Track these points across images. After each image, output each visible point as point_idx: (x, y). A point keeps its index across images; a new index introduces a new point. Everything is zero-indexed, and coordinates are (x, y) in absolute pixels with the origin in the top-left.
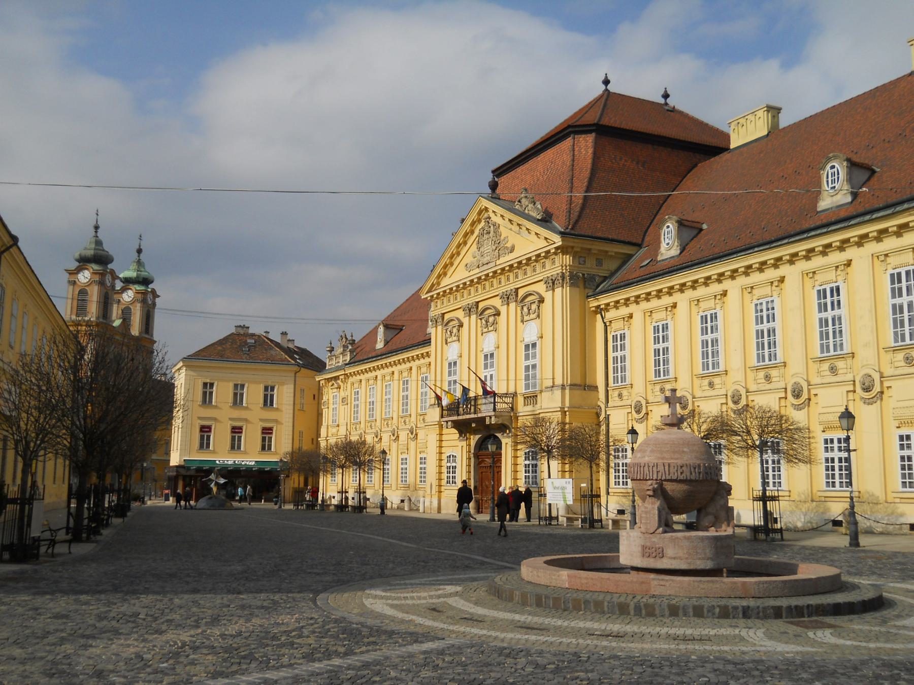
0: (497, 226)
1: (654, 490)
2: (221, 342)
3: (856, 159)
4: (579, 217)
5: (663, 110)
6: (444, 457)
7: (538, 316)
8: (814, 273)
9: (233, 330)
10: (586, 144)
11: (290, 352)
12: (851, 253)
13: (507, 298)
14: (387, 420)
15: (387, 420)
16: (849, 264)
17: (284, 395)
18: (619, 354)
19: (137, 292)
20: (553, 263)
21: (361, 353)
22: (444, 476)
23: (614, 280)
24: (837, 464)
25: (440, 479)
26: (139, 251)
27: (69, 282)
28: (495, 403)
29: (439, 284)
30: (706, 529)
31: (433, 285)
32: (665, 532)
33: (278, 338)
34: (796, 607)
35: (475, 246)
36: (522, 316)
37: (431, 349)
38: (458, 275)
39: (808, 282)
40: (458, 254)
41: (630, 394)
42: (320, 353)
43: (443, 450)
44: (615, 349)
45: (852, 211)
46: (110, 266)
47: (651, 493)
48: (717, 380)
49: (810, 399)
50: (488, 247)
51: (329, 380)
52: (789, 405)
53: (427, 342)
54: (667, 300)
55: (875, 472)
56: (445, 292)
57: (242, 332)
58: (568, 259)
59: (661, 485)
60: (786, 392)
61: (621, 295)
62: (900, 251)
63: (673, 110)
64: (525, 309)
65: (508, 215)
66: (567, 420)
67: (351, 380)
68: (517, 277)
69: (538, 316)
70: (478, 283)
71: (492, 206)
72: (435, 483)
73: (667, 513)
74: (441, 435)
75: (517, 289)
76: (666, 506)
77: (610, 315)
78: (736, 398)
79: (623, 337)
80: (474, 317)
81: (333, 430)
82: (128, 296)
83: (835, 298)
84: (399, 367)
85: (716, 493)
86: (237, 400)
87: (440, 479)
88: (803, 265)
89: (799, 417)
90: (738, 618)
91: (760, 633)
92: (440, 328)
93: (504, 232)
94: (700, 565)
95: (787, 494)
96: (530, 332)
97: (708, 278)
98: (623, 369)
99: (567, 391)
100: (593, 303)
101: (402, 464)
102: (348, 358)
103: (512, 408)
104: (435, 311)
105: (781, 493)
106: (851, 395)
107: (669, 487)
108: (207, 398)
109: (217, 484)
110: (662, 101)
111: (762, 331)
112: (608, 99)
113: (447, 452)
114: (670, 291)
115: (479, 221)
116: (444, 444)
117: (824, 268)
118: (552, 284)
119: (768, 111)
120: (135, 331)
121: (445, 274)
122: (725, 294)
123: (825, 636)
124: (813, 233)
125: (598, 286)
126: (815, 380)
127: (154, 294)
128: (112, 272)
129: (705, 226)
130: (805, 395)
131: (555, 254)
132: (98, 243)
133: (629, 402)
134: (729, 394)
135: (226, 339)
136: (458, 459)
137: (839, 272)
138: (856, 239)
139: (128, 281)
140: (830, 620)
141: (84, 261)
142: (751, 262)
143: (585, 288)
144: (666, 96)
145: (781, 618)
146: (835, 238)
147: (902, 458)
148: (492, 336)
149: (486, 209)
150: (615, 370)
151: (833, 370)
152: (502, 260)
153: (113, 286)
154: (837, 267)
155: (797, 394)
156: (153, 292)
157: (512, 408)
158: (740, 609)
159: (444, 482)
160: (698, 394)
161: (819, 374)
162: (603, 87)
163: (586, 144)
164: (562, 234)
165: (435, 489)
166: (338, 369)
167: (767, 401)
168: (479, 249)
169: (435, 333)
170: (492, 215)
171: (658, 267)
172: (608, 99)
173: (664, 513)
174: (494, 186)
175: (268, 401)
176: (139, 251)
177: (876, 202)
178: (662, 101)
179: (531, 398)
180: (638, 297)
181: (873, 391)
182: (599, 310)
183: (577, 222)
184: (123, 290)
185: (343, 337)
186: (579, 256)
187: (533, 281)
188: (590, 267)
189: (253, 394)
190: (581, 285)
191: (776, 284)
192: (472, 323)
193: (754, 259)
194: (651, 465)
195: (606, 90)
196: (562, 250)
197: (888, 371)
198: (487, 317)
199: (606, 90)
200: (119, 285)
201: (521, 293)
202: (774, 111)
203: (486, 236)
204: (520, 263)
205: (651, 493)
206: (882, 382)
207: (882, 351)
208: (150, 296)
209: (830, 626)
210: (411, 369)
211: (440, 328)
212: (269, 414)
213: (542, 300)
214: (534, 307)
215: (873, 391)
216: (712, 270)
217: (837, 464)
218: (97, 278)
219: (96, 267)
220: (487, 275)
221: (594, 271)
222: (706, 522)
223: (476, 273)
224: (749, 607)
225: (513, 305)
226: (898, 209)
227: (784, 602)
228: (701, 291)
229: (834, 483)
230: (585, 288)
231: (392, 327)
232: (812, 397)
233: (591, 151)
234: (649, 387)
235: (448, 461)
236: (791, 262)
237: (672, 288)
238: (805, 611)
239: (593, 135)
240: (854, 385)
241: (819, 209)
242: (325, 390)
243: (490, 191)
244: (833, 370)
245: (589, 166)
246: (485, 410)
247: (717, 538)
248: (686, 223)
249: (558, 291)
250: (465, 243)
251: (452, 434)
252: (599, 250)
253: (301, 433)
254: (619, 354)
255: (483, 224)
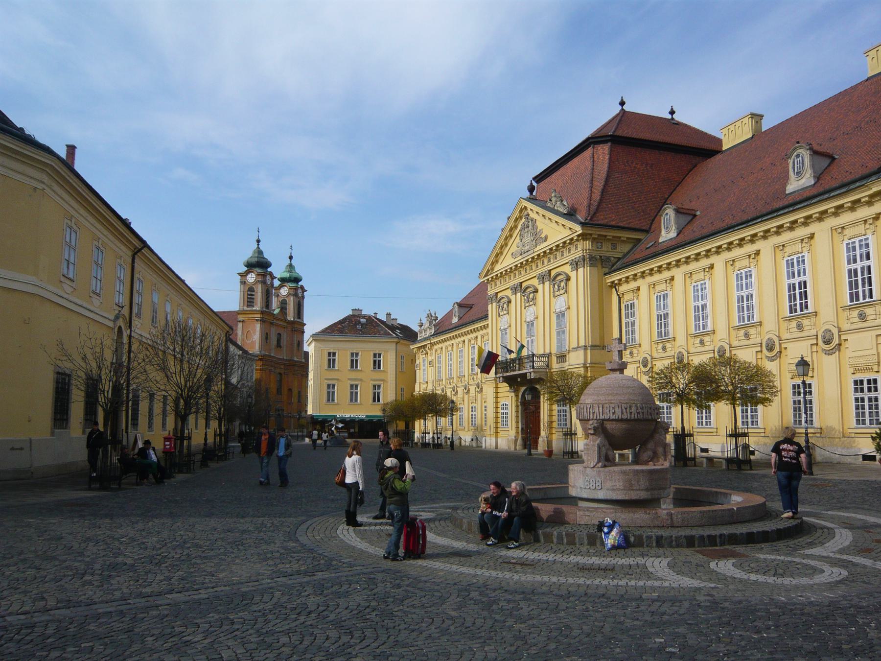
0: (534, 221)
1: (595, 429)
2: (341, 322)
3: (816, 147)
4: (597, 210)
5: (672, 124)
6: (500, 405)
7: (566, 291)
8: (783, 246)
9: (350, 313)
10: (603, 151)
11: (393, 328)
12: (813, 228)
13: (542, 279)
14: (461, 377)
15: (461, 377)
16: (812, 236)
17: (389, 361)
18: (630, 320)
19: (290, 288)
20: (576, 248)
21: (442, 328)
22: (500, 420)
23: (625, 260)
24: (866, 403)
25: (497, 423)
26: (291, 258)
27: (241, 282)
28: (533, 362)
29: (492, 269)
30: (646, 463)
31: (488, 271)
32: (605, 466)
33: (384, 319)
34: (709, 536)
35: (518, 238)
36: (554, 292)
37: (489, 321)
38: (507, 262)
39: (779, 254)
40: (506, 245)
41: (639, 352)
42: (415, 328)
43: (499, 400)
44: (627, 316)
45: (814, 192)
46: (269, 270)
47: (592, 432)
48: (706, 339)
49: (780, 352)
50: (528, 238)
51: (419, 348)
52: (764, 357)
53: (486, 317)
54: (666, 275)
55: (833, 408)
56: (497, 275)
57: (357, 313)
58: (588, 244)
59: (602, 424)
60: (761, 346)
61: (630, 272)
62: (854, 224)
63: (678, 124)
64: (556, 286)
65: (542, 211)
66: (589, 375)
67: (435, 347)
68: (549, 261)
69: (566, 291)
70: (521, 267)
71: (530, 205)
72: (493, 425)
73: (607, 450)
74: (497, 388)
75: (550, 271)
76: (607, 443)
77: (623, 288)
78: (721, 353)
79: (633, 306)
80: (518, 295)
81: (424, 386)
82: (284, 291)
83: (801, 266)
84: (469, 336)
85: (655, 431)
86: (354, 364)
87: (497, 423)
88: (775, 240)
89: (771, 367)
90: (651, 547)
91: (665, 562)
92: (494, 304)
93: (541, 224)
94: (633, 495)
95: (763, 431)
96: (560, 304)
97: (698, 254)
98: (633, 332)
99: (589, 351)
100: (610, 279)
101: (507, 413)
102: (433, 331)
103: (547, 366)
104: (491, 292)
105: (750, 430)
106: (814, 348)
107: (609, 426)
108: (331, 363)
109: (337, 428)
110: (669, 117)
111: (742, 297)
112: (624, 116)
113: (502, 401)
114: (669, 266)
115: (521, 217)
116: (500, 395)
117: (792, 242)
118: (575, 265)
119: (752, 118)
120: (290, 318)
121: (497, 261)
122: (712, 267)
123: (726, 567)
124: (782, 212)
125: (613, 266)
126: (785, 336)
127: (304, 290)
128: (271, 274)
129: (698, 213)
130: (777, 349)
131: (577, 240)
132: (260, 252)
133: (638, 358)
134: (716, 350)
135: (344, 320)
136: (509, 407)
137: (804, 245)
138: (817, 215)
139: (283, 280)
140: (740, 549)
141: (250, 266)
142: (732, 239)
143: (603, 267)
144: (672, 112)
145: (694, 546)
146: (800, 216)
147: (857, 400)
148: (532, 308)
149: (526, 208)
150: (627, 333)
151: (800, 327)
152: (539, 248)
153: (272, 284)
154: (802, 240)
155: (770, 348)
156: (302, 287)
157: (547, 366)
158: (654, 537)
159: (500, 425)
160: (692, 350)
161: (789, 330)
162: (620, 107)
163: (603, 151)
164: (583, 224)
165: (493, 430)
166: (426, 339)
167: (747, 356)
168: (521, 240)
169: (492, 309)
170: (530, 212)
171: (658, 249)
172: (624, 116)
173: (603, 449)
174: (531, 189)
175: (377, 364)
176: (291, 258)
177: (836, 183)
178: (669, 117)
179: (562, 358)
180: (643, 272)
181: (831, 343)
182: (613, 285)
183: (595, 214)
184: (281, 287)
185: (429, 315)
186: (597, 240)
187: (561, 264)
188: (606, 250)
189: (365, 362)
190: (600, 266)
191: (753, 256)
192: (517, 299)
193: (734, 237)
194: (588, 406)
195: (622, 109)
196: (583, 237)
197: (845, 326)
198: (527, 293)
199: (622, 109)
200: (277, 283)
201: (553, 273)
202: (757, 118)
203: (526, 230)
204: (551, 249)
205: (592, 432)
206: (840, 336)
207: (840, 310)
208: (300, 291)
209: (733, 555)
210: (477, 337)
211: (494, 304)
212: (377, 375)
213: (568, 279)
214: (563, 284)
215: (831, 343)
216: (701, 248)
217: (866, 403)
218: (260, 279)
219: (259, 270)
220: (527, 261)
221: (608, 254)
222: (645, 456)
223: (520, 259)
224: (662, 536)
225: (547, 284)
226: (852, 187)
227: (696, 532)
228: (693, 266)
229: (864, 421)
230: (603, 267)
231: (464, 306)
232: (783, 350)
233: (607, 157)
234: (654, 346)
235: (502, 409)
236: (765, 237)
237: (669, 264)
238: (718, 540)
239: (609, 144)
240: (817, 339)
241: (787, 192)
242: (417, 356)
243: (528, 194)
244: (800, 327)
245: (606, 169)
246: (527, 369)
247: (651, 472)
248: (682, 211)
249: (581, 270)
250: (511, 236)
251: (504, 387)
252: (614, 237)
253: (402, 389)
254: (630, 320)
255: (523, 220)
